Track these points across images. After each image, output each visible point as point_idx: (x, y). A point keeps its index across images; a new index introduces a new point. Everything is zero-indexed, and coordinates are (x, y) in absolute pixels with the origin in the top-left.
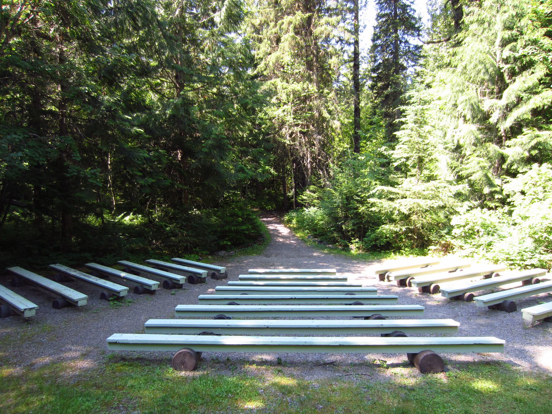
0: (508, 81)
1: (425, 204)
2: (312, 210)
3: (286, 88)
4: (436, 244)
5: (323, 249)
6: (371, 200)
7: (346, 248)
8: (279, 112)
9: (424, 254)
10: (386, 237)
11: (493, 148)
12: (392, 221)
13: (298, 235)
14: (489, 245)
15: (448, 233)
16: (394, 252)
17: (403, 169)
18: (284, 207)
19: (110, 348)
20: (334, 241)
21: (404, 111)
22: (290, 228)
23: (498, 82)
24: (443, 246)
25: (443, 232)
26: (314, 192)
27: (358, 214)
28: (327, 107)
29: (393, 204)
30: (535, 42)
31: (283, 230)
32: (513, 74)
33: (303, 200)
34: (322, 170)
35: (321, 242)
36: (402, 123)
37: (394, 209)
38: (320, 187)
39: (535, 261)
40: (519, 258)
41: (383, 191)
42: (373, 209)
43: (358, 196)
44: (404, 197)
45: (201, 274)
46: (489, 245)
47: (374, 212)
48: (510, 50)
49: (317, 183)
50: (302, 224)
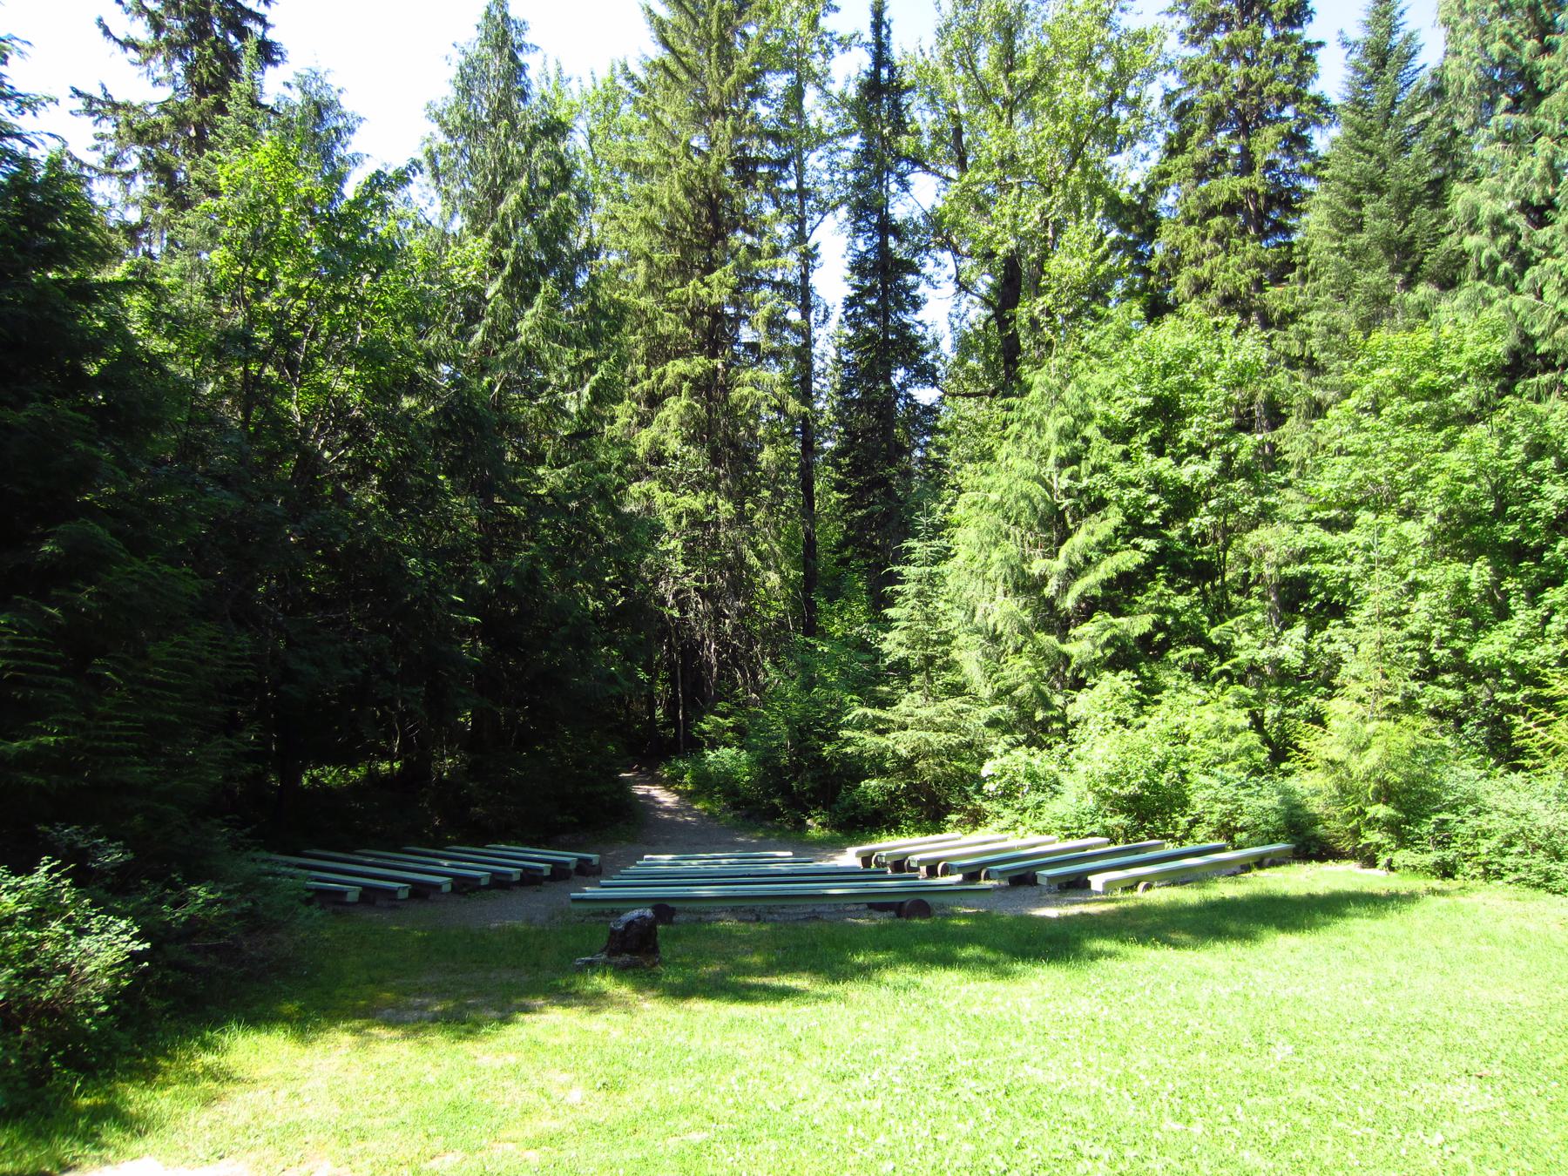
0: (1071, 527)
1: (938, 740)
2: (726, 753)
3: (672, 505)
4: (958, 812)
5: (755, 830)
6: (846, 733)
7: (800, 826)
8: (674, 572)
9: (940, 831)
10: (873, 802)
11: (1049, 640)
12: (883, 772)
13: (698, 807)
14: (1039, 806)
15: (979, 791)
16: (888, 830)
17: (903, 670)
18: (663, 748)
19: (572, 906)
20: (774, 813)
21: (900, 574)
22: (677, 792)
23: (1055, 525)
24: (970, 815)
25: (971, 789)
26: (725, 716)
27: (821, 759)
28: (753, 546)
29: (883, 741)
30: (1104, 469)
31: (666, 798)
32: (1079, 515)
33: (703, 732)
34: (741, 668)
35: (748, 817)
36: (899, 593)
37: (887, 747)
38: (738, 704)
39: (1096, 828)
40: (1076, 824)
41: (865, 715)
42: (849, 750)
43: (822, 726)
44: (903, 727)
45: (566, 863)
46: (1039, 806)
47: (851, 756)
48: (1070, 477)
49: (728, 696)
50: (706, 784)
